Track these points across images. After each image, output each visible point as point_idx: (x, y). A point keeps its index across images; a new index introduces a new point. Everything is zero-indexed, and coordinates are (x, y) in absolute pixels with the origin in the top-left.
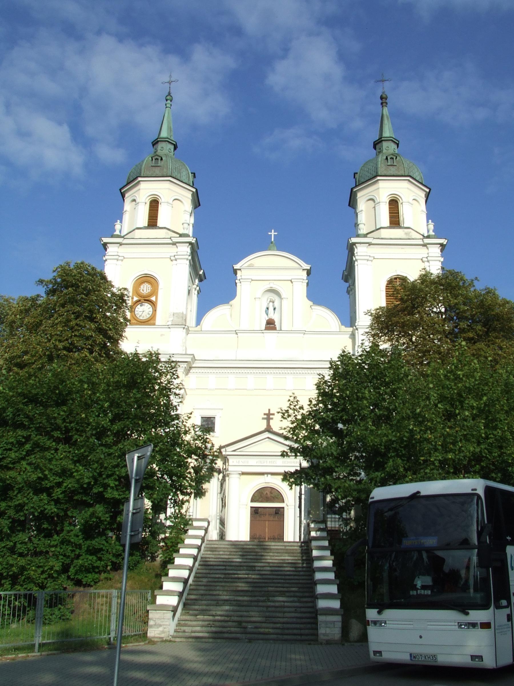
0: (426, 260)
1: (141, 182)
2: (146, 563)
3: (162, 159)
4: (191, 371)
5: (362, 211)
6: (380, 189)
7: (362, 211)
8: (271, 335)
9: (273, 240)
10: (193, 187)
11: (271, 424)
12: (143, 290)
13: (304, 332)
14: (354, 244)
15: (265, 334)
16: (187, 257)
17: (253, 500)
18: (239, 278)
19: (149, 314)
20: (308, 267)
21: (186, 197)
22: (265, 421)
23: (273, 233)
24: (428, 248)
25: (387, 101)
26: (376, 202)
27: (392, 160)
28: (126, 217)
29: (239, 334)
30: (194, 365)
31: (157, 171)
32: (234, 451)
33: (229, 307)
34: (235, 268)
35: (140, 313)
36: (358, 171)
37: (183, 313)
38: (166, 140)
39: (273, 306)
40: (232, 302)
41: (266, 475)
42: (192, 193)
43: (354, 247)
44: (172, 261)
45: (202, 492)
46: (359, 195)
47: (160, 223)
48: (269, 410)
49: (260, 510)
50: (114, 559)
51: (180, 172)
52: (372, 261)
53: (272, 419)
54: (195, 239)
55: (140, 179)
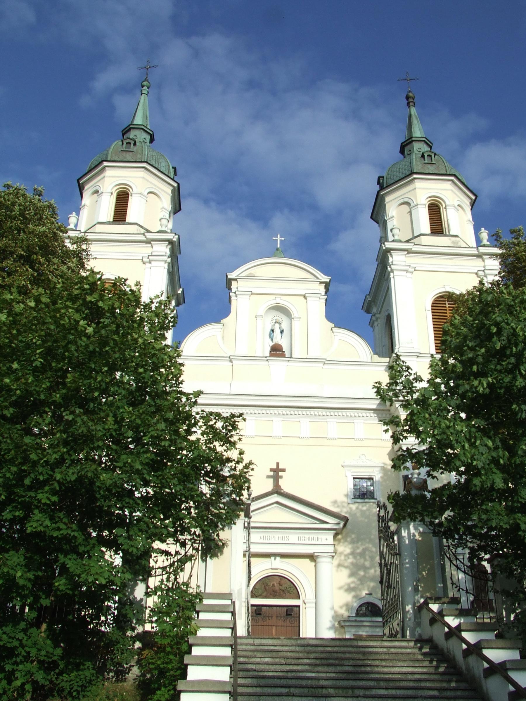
0: (483, 274)
1: (107, 169)
2: (106, 683)
3: (135, 144)
5: (393, 217)
6: (417, 190)
7: (393, 217)
8: (277, 364)
9: (279, 246)
10: (173, 179)
11: (280, 483)
13: (324, 361)
14: (389, 250)
15: (271, 363)
16: (165, 258)
17: (254, 594)
18: (233, 290)
20: (327, 279)
21: (165, 192)
22: (271, 480)
23: (279, 238)
24: (483, 260)
25: (414, 101)
26: (412, 205)
27: (429, 158)
28: (85, 213)
29: (234, 362)
31: (129, 157)
34: (229, 277)
36: (384, 174)
38: (140, 128)
39: (280, 328)
40: (224, 321)
41: (273, 558)
42: (172, 188)
43: (389, 255)
44: (144, 263)
45: (217, 545)
46: (387, 199)
47: (130, 217)
48: (278, 464)
50: (40, 677)
51: (157, 161)
52: (412, 273)
53: (281, 477)
54: (177, 237)
55: (105, 164)
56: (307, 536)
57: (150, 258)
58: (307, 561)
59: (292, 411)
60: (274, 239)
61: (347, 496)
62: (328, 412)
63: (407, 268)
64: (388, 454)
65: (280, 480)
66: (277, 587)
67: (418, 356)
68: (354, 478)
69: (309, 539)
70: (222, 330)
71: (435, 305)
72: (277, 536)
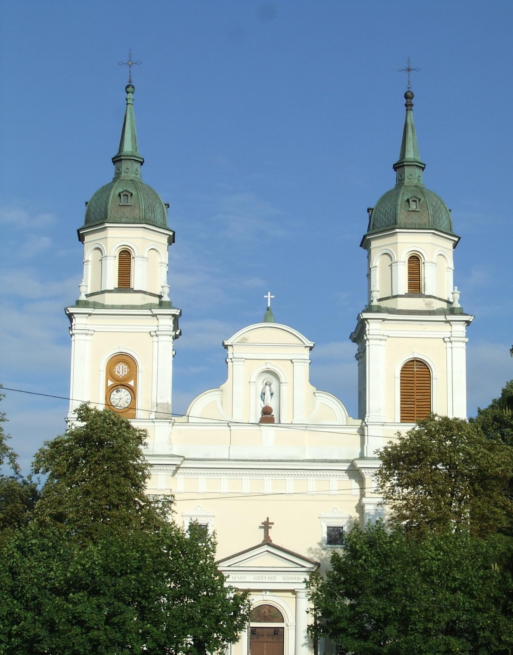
0: (449, 340)
1: (108, 228)
3: (132, 195)
4: (178, 472)
5: (376, 267)
8: (267, 430)
9: (269, 305)
12: (118, 372)
14: (366, 319)
18: (230, 356)
19: (127, 402)
22: (263, 530)
23: (269, 296)
30: (181, 466)
32: (229, 566)
33: (220, 393)
35: (117, 401)
37: (168, 403)
39: (270, 391)
40: (223, 387)
41: (264, 592)
43: (366, 322)
48: (268, 519)
49: (257, 630)
52: (386, 340)
56: (290, 576)
57: (158, 333)
58: (290, 594)
59: (279, 472)
60: (265, 297)
61: (320, 544)
62: (308, 473)
63: (381, 337)
64: (356, 507)
65: (269, 529)
66: (267, 613)
67: (383, 425)
68: (328, 527)
69: (291, 578)
70: (220, 396)
71: (404, 369)
72: (267, 576)
